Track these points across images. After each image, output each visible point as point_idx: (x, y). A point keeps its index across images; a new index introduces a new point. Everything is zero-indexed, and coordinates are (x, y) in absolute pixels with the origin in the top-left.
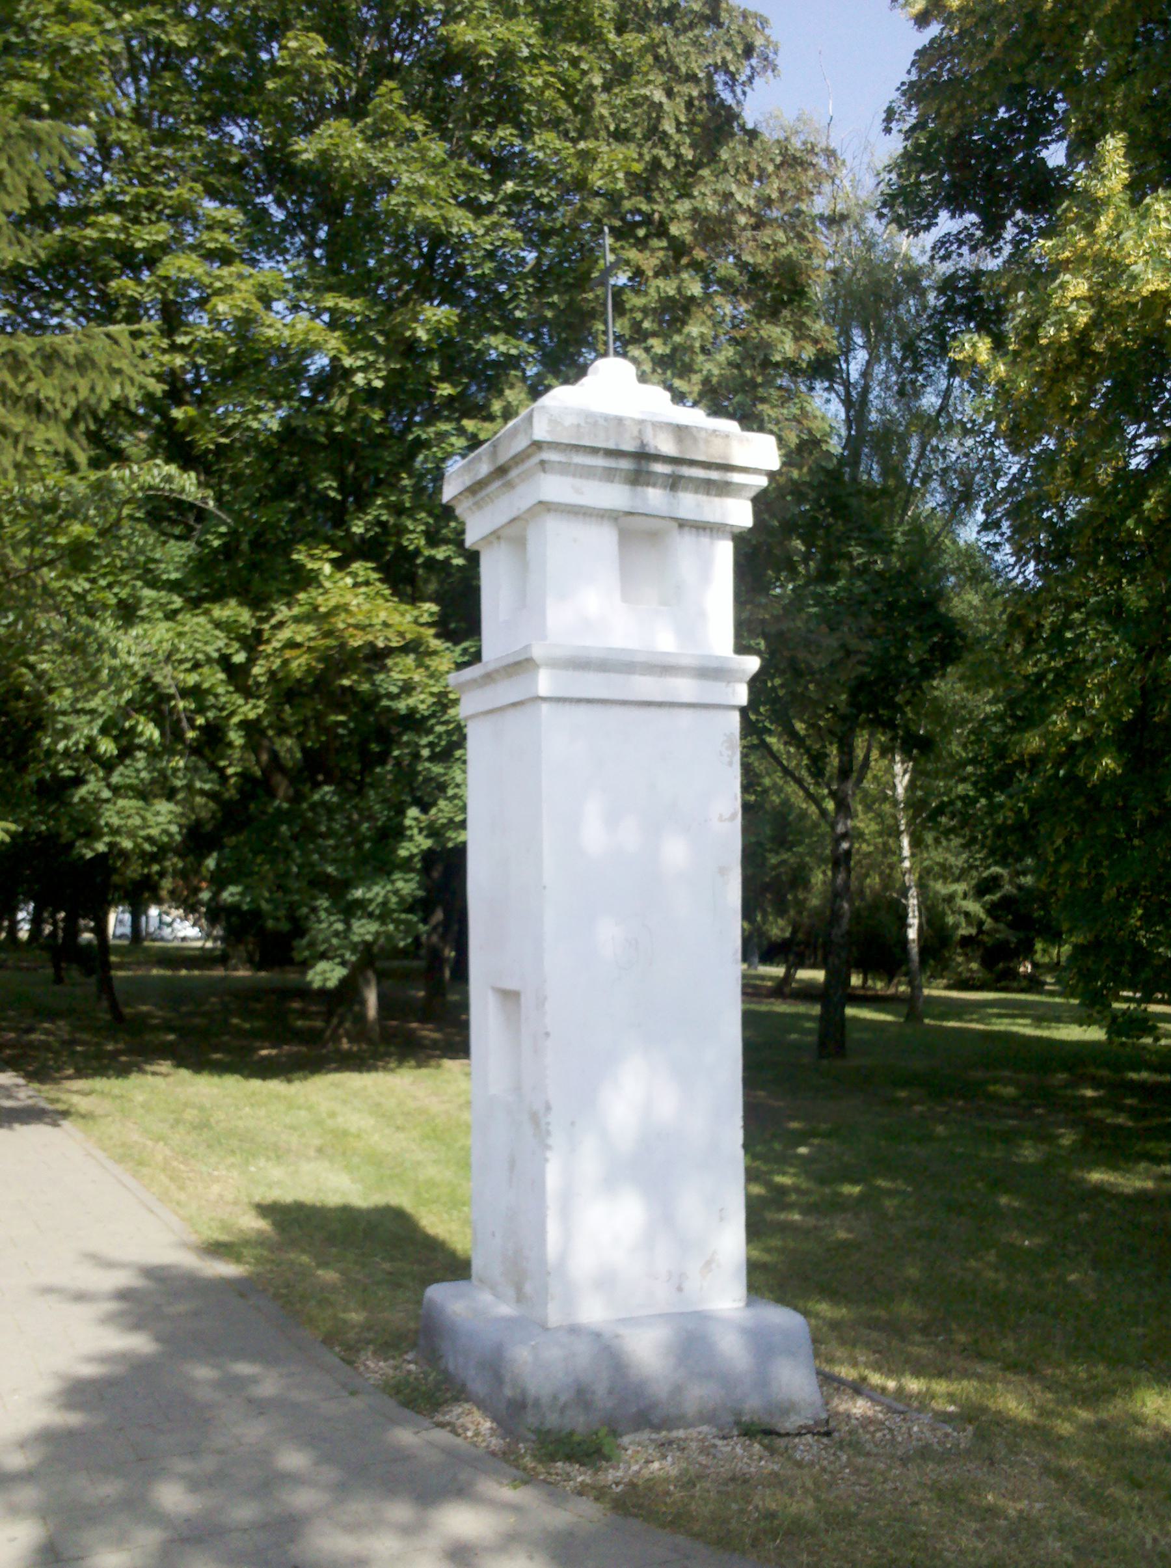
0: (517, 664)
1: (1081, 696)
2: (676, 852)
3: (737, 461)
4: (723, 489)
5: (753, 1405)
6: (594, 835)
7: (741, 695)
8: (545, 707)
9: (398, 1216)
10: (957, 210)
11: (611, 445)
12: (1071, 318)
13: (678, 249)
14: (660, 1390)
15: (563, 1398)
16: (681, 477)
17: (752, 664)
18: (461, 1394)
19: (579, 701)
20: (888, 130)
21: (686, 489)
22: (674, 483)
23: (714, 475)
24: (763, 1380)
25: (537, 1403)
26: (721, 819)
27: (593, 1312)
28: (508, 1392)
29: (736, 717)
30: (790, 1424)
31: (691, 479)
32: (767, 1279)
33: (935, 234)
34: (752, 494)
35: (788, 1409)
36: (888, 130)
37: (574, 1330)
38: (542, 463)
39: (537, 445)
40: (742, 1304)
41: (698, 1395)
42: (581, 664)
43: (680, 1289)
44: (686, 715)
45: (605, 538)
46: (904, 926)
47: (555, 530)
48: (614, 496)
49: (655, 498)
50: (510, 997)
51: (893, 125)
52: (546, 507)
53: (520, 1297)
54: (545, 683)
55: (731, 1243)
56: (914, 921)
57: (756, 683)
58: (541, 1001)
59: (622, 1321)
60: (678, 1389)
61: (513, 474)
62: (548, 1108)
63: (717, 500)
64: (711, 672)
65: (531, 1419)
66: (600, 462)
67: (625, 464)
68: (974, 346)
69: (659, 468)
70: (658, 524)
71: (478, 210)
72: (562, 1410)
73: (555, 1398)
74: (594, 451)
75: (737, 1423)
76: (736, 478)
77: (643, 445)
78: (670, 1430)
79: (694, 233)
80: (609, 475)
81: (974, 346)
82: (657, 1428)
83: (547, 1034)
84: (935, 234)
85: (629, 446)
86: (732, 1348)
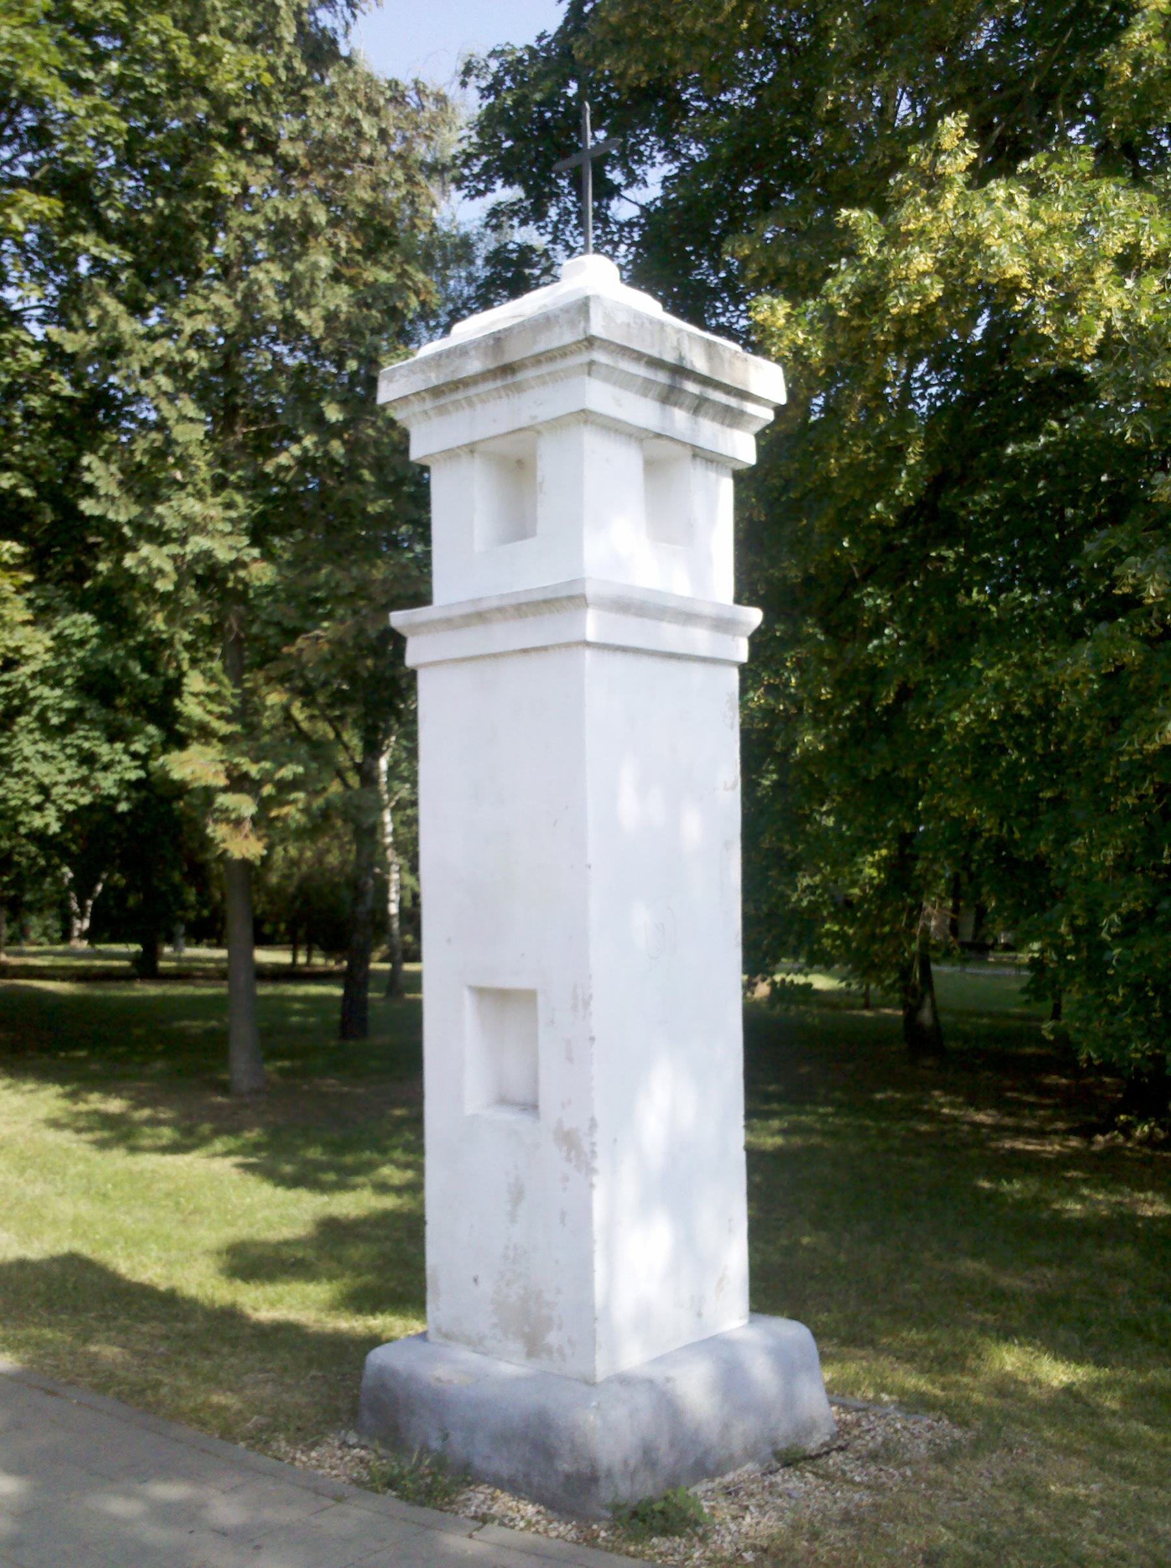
0: (571, 598)
1: (777, 674)
2: (692, 826)
3: (754, 390)
4: (732, 418)
5: (784, 1431)
6: (628, 807)
7: (742, 653)
8: (588, 653)
9: (73, 1263)
10: (508, 183)
11: (654, 353)
12: (921, 290)
13: (287, 166)
14: (711, 1434)
15: (632, 1463)
16: (707, 400)
17: (754, 616)
18: (468, 1476)
19: (624, 649)
20: (464, 84)
21: (706, 415)
22: (699, 406)
23: (733, 402)
24: (789, 1400)
25: (609, 1474)
26: (726, 789)
27: (633, 1357)
28: (565, 1466)
29: (734, 676)
30: (813, 1445)
31: (714, 403)
32: (771, 1290)
33: (490, 200)
34: (757, 428)
35: (809, 1428)
36: (464, 84)
37: (624, 1380)
38: (591, 363)
39: (590, 342)
40: (745, 1321)
41: (744, 1430)
42: (626, 606)
43: (699, 1315)
44: (698, 669)
45: (626, 460)
46: (386, 901)
47: (593, 443)
48: (643, 412)
49: (680, 420)
50: (504, 1002)
51: (472, 80)
52: (585, 416)
53: (534, 1347)
54: (592, 626)
55: (735, 1257)
56: (393, 895)
57: (758, 641)
58: (581, 1002)
59: (660, 1360)
60: (726, 1426)
61: (520, 377)
62: (593, 1124)
63: (728, 430)
64: (722, 625)
65: (605, 1493)
66: (641, 371)
67: (662, 378)
68: (772, 307)
69: (691, 387)
70: (678, 449)
71: (80, 86)
72: (633, 1475)
73: (626, 1463)
74: (638, 356)
75: (776, 1454)
76: (750, 408)
77: (681, 358)
78: (722, 1475)
79: (307, 155)
80: (646, 387)
81: (772, 307)
82: (711, 1476)
83: (592, 1039)
84: (490, 200)
85: (670, 358)
86: (762, 1371)
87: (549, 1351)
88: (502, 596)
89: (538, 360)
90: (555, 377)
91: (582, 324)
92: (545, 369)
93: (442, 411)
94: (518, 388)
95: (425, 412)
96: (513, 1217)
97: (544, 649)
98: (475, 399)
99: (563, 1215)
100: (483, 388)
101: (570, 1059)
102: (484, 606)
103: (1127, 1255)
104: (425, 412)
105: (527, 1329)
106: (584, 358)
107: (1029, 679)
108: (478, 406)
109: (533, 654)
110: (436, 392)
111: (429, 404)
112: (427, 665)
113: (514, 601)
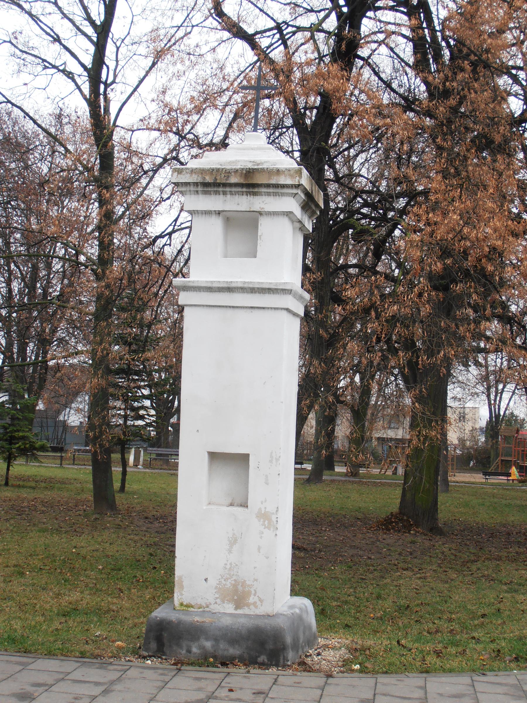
87: (248, 605)
88: (245, 283)
89: (268, 186)
90: (275, 194)
91: (298, 178)
92: (271, 190)
93: (205, 193)
94: (255, 194)
95: (197, 192)
96: (230, 551)
97: (264, 308)
98: (228, 193)
99: (259, 548)
100: (234, 189)
101: (267, 484)
102: (233, 285)
103: (316, 9)
104: (197, 192)
105: (236, 598)
106: (294, 191)
107: (137, 218)
108: (229, 196)
109: (256, 310)
110: (205, 185)
111: (200, 189)
112: (187, 305)
113: (251, 286)
